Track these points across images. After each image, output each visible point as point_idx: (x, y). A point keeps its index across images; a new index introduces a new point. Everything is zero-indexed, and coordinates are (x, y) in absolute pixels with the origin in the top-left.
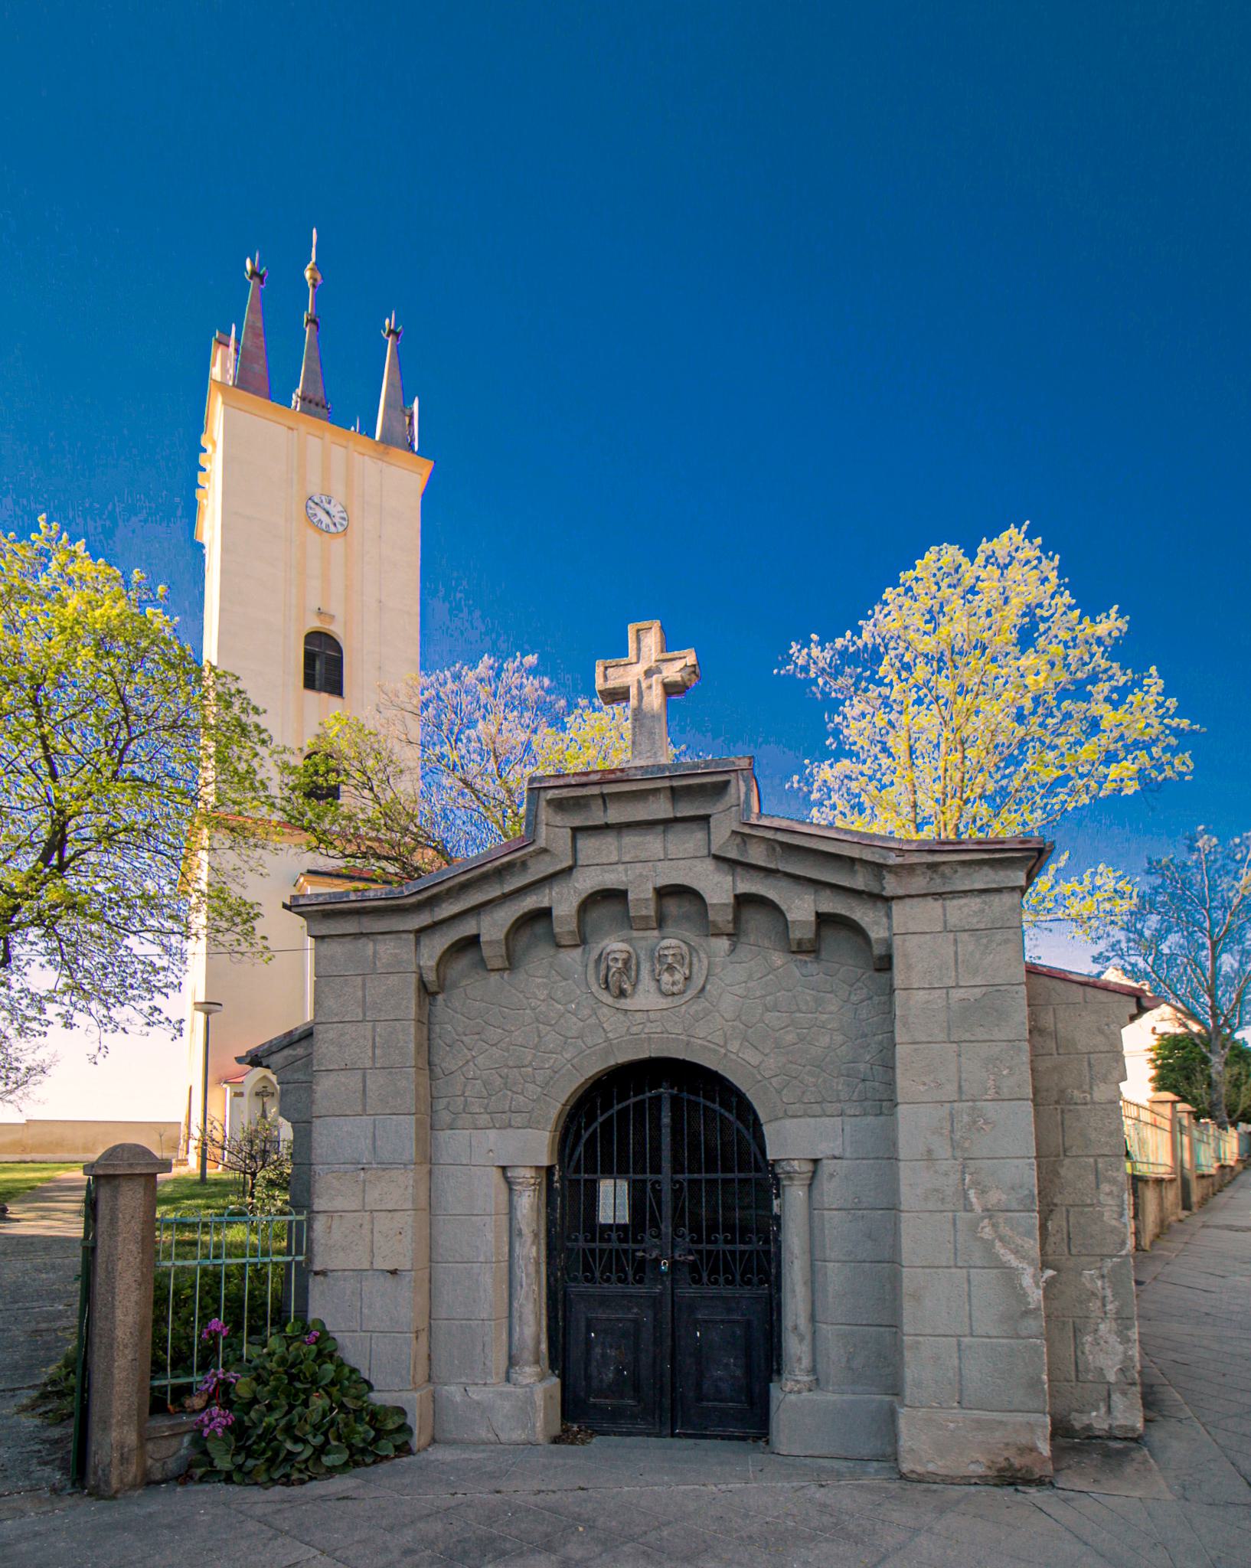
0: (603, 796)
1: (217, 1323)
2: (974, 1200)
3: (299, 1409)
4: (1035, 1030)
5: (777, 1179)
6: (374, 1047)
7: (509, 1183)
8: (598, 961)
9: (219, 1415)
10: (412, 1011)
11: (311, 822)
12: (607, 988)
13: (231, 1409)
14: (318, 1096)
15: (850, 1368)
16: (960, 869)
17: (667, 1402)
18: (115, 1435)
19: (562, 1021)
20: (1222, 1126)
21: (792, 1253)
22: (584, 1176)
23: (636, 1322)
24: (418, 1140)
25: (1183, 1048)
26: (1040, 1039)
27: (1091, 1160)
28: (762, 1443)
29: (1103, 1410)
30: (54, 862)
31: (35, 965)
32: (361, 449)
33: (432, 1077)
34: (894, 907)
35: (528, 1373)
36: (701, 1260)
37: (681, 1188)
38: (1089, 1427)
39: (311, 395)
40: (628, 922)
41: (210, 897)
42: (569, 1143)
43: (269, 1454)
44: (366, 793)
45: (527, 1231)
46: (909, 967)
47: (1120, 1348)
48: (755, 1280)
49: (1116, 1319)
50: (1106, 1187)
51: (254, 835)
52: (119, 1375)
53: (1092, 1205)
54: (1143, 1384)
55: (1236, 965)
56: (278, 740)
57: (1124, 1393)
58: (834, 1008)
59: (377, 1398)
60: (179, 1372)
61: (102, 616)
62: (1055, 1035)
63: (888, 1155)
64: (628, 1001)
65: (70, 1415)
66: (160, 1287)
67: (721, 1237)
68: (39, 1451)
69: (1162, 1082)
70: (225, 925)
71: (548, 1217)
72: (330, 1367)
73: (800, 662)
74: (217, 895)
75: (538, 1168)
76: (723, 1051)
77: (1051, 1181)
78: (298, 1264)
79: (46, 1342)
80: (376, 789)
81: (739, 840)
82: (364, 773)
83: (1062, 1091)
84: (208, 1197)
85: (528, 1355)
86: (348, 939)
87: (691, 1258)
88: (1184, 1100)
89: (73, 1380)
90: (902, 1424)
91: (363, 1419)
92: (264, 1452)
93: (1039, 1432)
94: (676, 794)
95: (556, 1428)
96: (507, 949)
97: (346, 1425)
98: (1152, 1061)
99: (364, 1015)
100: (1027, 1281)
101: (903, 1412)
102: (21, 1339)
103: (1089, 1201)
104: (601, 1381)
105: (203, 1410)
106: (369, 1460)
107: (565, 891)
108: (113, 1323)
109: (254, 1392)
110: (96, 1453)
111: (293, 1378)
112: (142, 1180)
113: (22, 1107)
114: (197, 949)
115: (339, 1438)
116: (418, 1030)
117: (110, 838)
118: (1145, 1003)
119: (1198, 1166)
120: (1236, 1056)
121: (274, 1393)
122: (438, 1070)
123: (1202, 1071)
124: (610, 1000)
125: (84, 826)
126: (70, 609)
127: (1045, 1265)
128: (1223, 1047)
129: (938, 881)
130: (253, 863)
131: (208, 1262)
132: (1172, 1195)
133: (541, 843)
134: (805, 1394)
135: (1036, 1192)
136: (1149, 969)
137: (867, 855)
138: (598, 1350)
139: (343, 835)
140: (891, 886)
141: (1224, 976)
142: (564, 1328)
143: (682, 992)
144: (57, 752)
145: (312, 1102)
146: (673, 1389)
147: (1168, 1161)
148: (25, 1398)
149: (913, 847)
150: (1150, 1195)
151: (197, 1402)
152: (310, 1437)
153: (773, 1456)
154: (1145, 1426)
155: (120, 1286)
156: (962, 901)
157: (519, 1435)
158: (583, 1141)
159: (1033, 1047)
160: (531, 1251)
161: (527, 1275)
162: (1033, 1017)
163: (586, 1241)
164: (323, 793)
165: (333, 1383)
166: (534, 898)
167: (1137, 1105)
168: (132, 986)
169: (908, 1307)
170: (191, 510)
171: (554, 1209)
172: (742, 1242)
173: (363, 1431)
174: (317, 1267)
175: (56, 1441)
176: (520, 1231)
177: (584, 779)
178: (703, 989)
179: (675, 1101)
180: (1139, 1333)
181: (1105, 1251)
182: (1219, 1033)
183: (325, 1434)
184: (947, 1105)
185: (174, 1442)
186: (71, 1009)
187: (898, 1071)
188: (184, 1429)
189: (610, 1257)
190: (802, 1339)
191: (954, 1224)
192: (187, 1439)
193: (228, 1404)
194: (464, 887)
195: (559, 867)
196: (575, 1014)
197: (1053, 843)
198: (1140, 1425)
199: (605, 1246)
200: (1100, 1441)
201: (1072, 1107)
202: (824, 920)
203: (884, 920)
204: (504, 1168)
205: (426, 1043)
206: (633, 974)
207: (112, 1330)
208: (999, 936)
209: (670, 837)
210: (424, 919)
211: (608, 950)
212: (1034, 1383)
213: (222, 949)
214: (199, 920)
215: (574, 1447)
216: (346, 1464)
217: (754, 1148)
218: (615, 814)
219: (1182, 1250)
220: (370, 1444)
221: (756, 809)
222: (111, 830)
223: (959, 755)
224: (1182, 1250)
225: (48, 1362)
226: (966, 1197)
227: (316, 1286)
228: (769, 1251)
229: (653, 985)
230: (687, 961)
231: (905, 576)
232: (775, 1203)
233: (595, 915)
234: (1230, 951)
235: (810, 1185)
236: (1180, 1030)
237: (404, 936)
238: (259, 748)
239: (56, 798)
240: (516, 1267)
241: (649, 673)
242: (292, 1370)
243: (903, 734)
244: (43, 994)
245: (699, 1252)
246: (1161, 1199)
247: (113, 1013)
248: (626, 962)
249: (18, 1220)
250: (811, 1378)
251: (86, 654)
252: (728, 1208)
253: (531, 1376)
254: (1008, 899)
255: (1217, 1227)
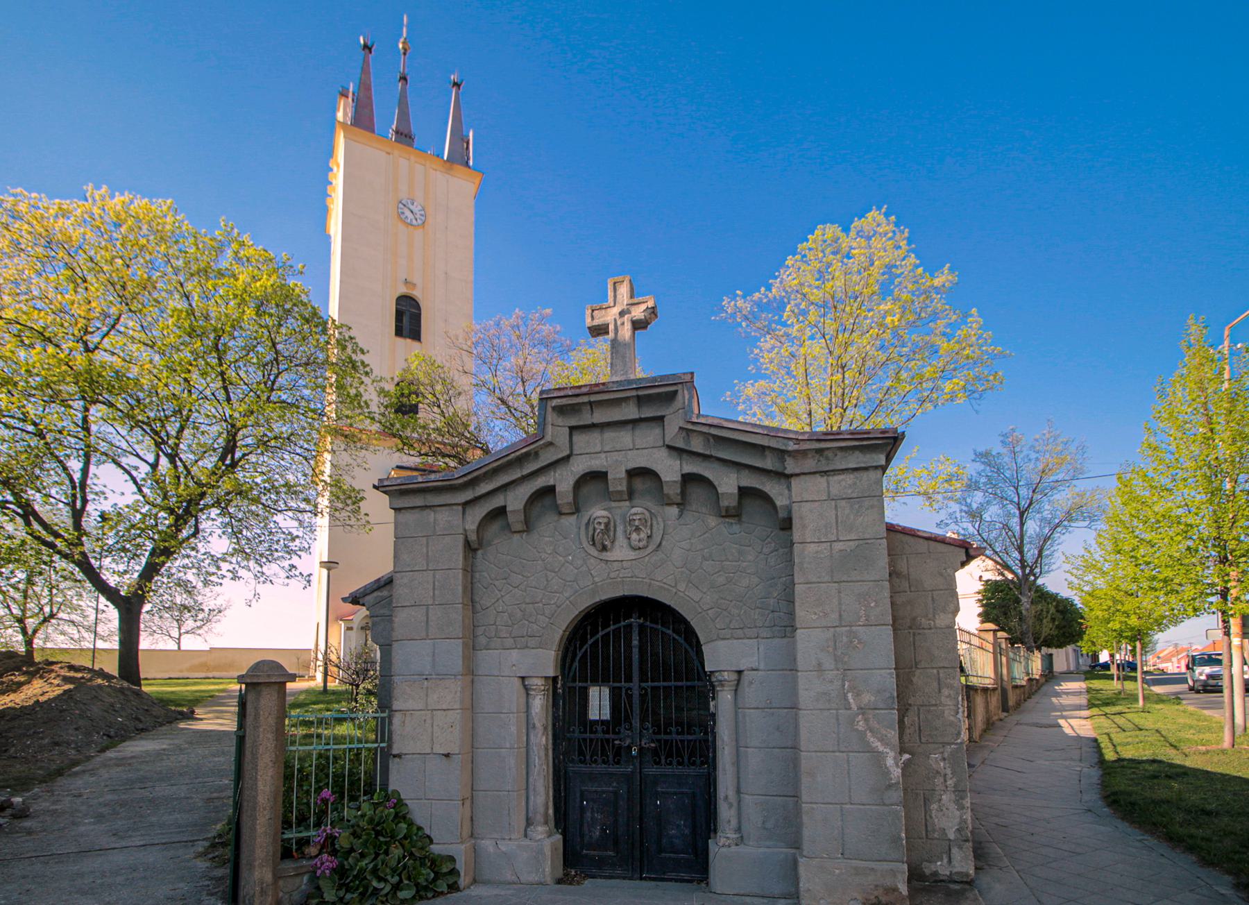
0: (590, 403)
1: (326, 793)
2: (851, 701)
3: (382, 857)
4: (894, 574)
5: (713, 687)
6: (434, 589)
7: (527, 689)
8: (588, 524)
9: (327, 860)
10: (460, 564)
11: (398, 430)
12: (594, 544)
13: (335, 856)
14: (395, 625)
15: (765, 828)
16: (839, 454)
17: (637, 853)
18: (257, 874)
19: (563, 569)
20: (1030, 649)
21: (723, 740)
22: (578, 684)
23: (615, 793)
24: (464, 658)
25: (1001, 591)
26: (898, 580)
27: (935, 671)
28: (703, 885)
29: (945, 860)
30: (228, 462)
31: (215, 536)
32: (434, 167)
33: (474, 612)
34: (793, 482)
35: (540, 831)
36: (660, 746)
37: (646, 694)
38: (935, 874)
39: (401, 130)
40: (609, 496)
41: (331, 486)
42: (568, 660)
43: (361, 890)
44: (436, 409)
45: (538, 725)
46: (804, 527)
47: (958, 813)
48: (698, 762)
49: (954, 792)
50: (946, 692)
51: (360, 440)
52: (260, 830)
53: (936, 705)
54: (974, 842)
55: (1038, 529)
56: (377, 372)
57: (960, 848)
58: (750, 558)
59: (435, 849)
60: (302, 828)
61: (261, 286)
62: (908, 577)
63: (792, 667)
64: (608, 554)
65: (229, 860)
66: (288, 766)
67: (673, 729)
68: (208, 886)
69: (986, 617)
70: (340, 505)
71: (554, 713)
72: (403, 826)
73: (729, 311)
74: (336, 484)
75: (546, 678)
76: (674, 590)
77: (907, 687)
78: (382, 749)
79: (217, 807)
80: (442, 406)
81: (684, 434)
82: (434, 395)
83: (914, 619)
84: (328, 702)
85: (540, 818)
86: (417, 510)
87: (653, 745)
88: (1002, 629)
89: (231, 836)
90: (802, 870)
91: (425, 865)
92: (357, 889)
93: (900, 877)
94: (641, 401)
95: (560, 873)
96: (525, 516)
97: (414, 868)
98: (980, 601)
99: (428, 565)
100: (890, 762)
101: (801, 861)
102: (200, 805)
103: (934, 702)
104: (591, 837)
105: (316, 856)
106: (430, 895)
107: (565, 473)
108: (256, 791)
109: (351, 843)
110: (244, 887)
111: (378, 834)
112: (276, 687)
113: (207, 638)
114: (323, 522)
115: (409, 878)
116: (465, 576)
117: (265, 443)
118: (972, 552)
119: (1013, 679)
120: (1039, 597)
121: (365, 844)
122: (478, 606)
123: (1015, 609)
124: (595, 553)
125: (246, 438)
126: (240, 282)
127: (902, 751)
128: (1030, 590)
129: (824, 462)
130: (359, 460)
131: (320, 747)
132: (995, 700)
133: (548, 438)
134: (733, 848)
135: (895, 694)
136: (976, 533)
137: (773, 444)
138: (589, 814)
139: (420, 441)
140: (791, 466)
141: (1029, 537)
142: (565, 796)
143: (645, 547)
144: (231, 384)
145: (392, 629)
146: (642, 844)
147: (992, 676)
148: (201, 847)
149: (806, 437)
150: (979, 700)
151: (313, 850)
152: (389, 877)
153: (711, 895)
154: (976, 873)
155: (261, 764)
156: (841, 477)
157: (534, 878)
158: (578, 658)
159: (892, 586)
160: (541, 740)
161: (539, 758)
162: (892, 563)
163: (580, 732)
164: (405, 408)
165: (405, 837)
166: (544, 478)
167: (968, 633)
168: (276, 550)
169: (805, 781)
170: (325, 211)
171: (558, 709)
172: (689, 733)
173: (426, 873)
174: (395, 752)
175: (220, 879)
176: (534, 725)
177: (578, 391)
178: (660, 544)
179: (642, 628)
180: (971, 803)
181: (946, 740)
182: (1027, 579)
183: (400, 875)
184: (832, 630)
185: (298, 880)
186: (237, 567)
187: (797, 604)
188: (304, 870)
189: (597, 742)
190: (731, 805)
191: (838, 719)
192: (306, 878)
193: (334, 852)
194: (496, 471)
195: (560, 456)
196: (571, 564)
197: (903, 433)
198: (972, 872)
199: (593, 736)
200: (943, 884)
201: (921, 631)
202: (744, 492)
203: (786, 492)
204: (523, 678)
205: (470, 586)
206: (612, 534)
207: (255, 797)
208: (867, 503)
209: (638, 432)
210: (468, 495)
211: (594, 516)
212: (895, 840)
213: (339, 523)
214: (324, 502)
215: (572, 887)
216: (414, 897)
217: (696, 663)
218: (600, 416)
219: (1002, 742)
220: (431, 883)
221: (696, 411)
222: (266, 439)
223: (840, 376)
224: (1002, 742)
225: (219, 820)
226: (846, 699)
227: (394, 765)
228: (708, 740)
229: (626, 542)
230: (649, 524)
231: (801, 247)
232: (712, 704)
233: (585, 490)
234: (1033, 518)
235: (736, 690)
236: (999, 578)
237: (455, 507)
238: (364, 379)
239: (230, 416)
240: (531, 753)
241: (622, 314)
242: (378, 827)
243: (802, 361)
244: (219, 556)
245: (659, 741)
246: (987, 703)
247: (265, 569)
248: (607, 525)
249: (201, 719)
250: (737, 836)
251: (250, 312)
252: (679, 709)
253: (542, 833)
254: (873, 475)
255: (1026, 724)
